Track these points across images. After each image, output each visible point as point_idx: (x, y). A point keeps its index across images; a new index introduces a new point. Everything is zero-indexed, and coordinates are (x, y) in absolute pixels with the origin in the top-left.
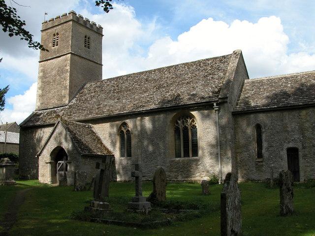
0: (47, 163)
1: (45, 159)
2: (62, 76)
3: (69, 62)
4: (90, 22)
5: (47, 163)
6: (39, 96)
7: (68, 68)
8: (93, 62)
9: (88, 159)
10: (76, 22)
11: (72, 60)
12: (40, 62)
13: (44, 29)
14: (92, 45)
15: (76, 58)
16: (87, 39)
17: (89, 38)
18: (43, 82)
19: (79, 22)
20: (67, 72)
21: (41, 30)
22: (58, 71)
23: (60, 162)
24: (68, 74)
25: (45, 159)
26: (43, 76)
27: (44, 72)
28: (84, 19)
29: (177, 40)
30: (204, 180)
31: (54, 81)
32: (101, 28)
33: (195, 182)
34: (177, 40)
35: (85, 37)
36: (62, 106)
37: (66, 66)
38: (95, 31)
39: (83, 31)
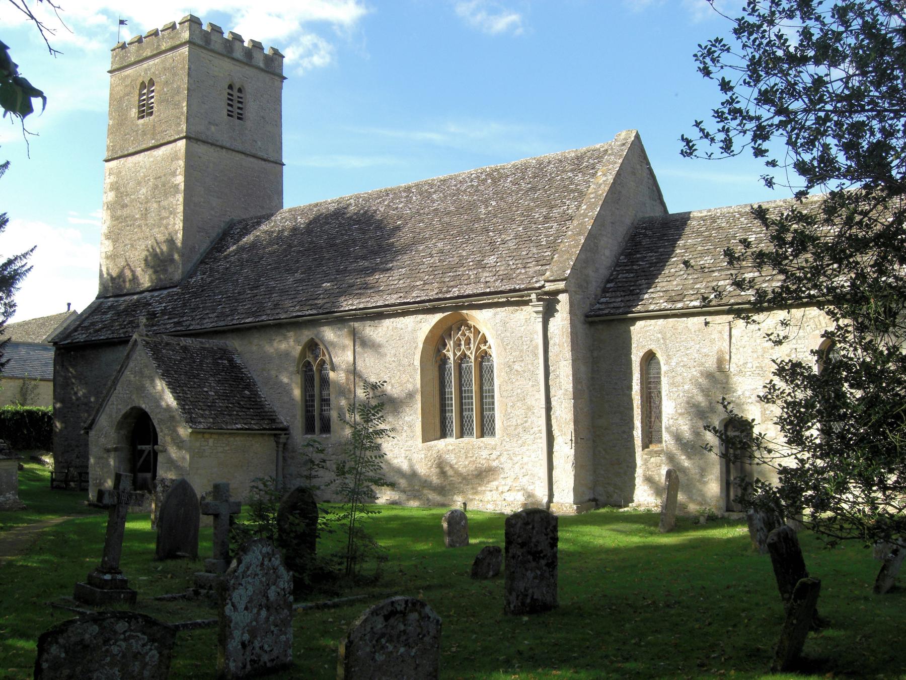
0: (108, 451)
1: (102, 440)
2: (164, 203)
3: (182, 163)
4: (243, 41)
5: (108, 451)
6: (107, 258)
7: (180, 180)
8: (254, 156)
9: (211, 441)
10: (247, 64)
11: (189, 156)
12: (107, 161)
13: (116, 66)
14: (252, 109)
15: (202, 149)
16: (236, 93)
17: (240, 90)
18: (115, 218)
19: (212, 47)
20: (177, 191)
21: (109, 69)
22: (156, 187)
23: (144, 447)
24: (180, 197)
25: (102, 440)
26: (116, 202)
27: (117, 189)
28: (246, 44)
29: (756, 157)
30: (456, 511)
31: (145, 215)
32: (277, 56)
33: (829, 671)
34: (756, 157)
35: (230, 87)
36: (166, 288)
37: (174, 174)
38: (258, 68)
39: (224, 69)
